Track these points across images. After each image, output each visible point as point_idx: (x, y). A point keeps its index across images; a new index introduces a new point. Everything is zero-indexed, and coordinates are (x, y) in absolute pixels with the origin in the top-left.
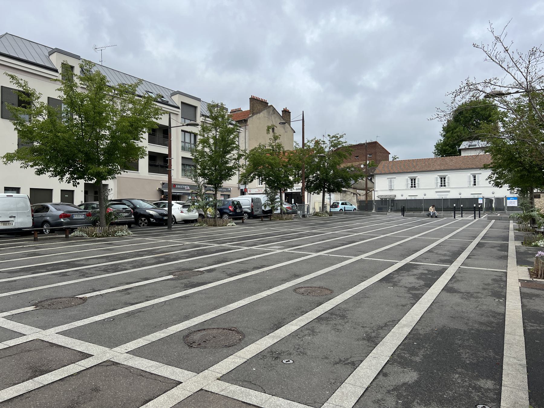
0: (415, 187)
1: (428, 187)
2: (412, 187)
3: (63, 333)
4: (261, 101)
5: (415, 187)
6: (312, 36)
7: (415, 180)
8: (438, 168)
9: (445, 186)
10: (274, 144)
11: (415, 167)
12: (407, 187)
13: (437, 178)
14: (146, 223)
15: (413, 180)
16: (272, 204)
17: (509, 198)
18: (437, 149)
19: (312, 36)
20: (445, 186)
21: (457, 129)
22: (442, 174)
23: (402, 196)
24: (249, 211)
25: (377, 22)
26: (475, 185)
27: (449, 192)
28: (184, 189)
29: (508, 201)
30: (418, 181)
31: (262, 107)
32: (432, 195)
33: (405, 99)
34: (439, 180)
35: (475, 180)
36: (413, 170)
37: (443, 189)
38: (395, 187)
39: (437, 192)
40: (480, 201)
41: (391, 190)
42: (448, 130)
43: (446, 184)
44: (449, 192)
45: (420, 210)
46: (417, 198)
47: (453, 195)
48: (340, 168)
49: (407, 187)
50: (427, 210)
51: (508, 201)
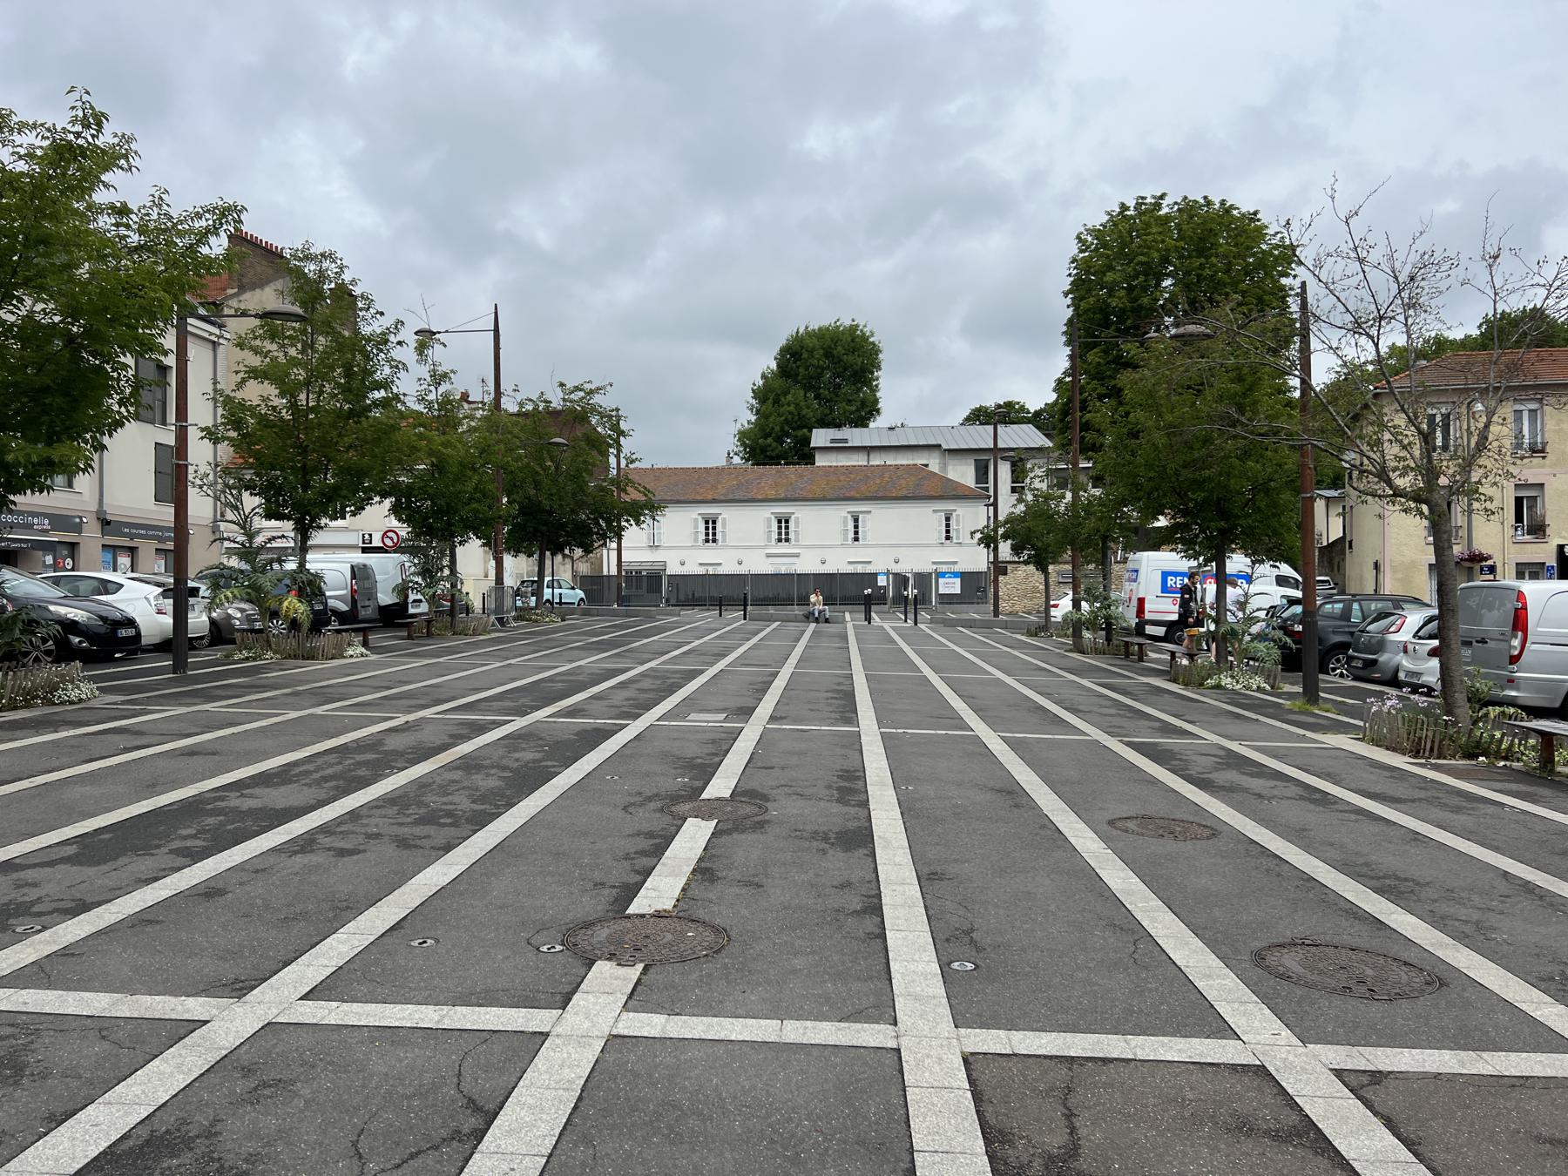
0: (714, 541)
1: (746, 543)
2: (707, 541)
3: (1224, 1030)
4: (265, 249)
5: (714, 541)
6: (362, 55)
7: (787, 521)
8: (772, 493)
9: (787, 540)
10: (432, 397)
11: (714, 487)
12: (696, 540)
13: (769, 520)
14: (48, 653)
15: (711, 523)
16: (428, 586)
17: (943, 575)
18: (743, 444)
19: (362, 55)
20: (787, 540)
21: (789, 397)
22: (782, 509)
23: (740, 563)
24: (344, 607)
25: (572, 55)
26: (856, 539)
27: (797, 556)
28: (30, 527)
29: (941, 581)
30: (724, 525)
31: (270, 271)
32: (758, 564)
33: (626, 291)
34: (775, 525)
35: (856, 527)
36: (710, 497)
37: (783, 548)
38: (664, 540)
39: (768, 556)
40: (882, 581)
41: (654, 547)
42: (766, 395)
43: (792, 536)
44: (797, 556)
45: (787, 601)
46: (721, 571)
47: (808, 564)
48: (546, 483)
49: (696, 540)
50: (804, 601)
51: (941, 581)
